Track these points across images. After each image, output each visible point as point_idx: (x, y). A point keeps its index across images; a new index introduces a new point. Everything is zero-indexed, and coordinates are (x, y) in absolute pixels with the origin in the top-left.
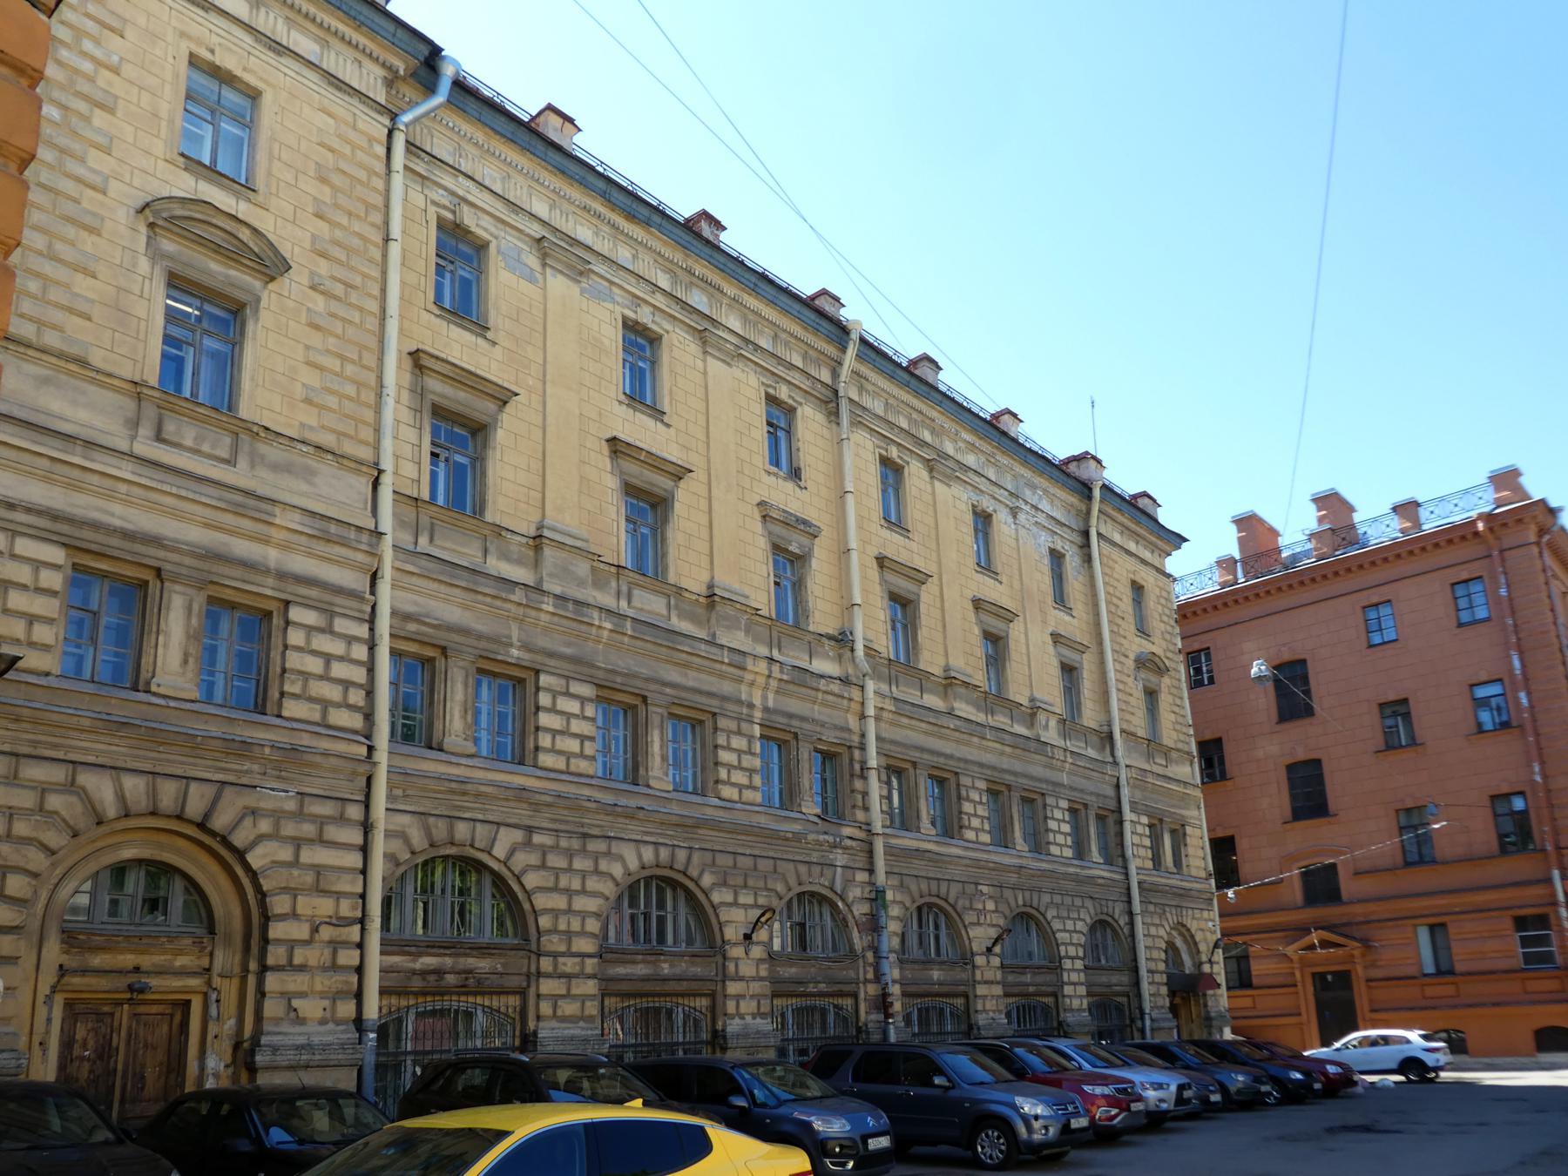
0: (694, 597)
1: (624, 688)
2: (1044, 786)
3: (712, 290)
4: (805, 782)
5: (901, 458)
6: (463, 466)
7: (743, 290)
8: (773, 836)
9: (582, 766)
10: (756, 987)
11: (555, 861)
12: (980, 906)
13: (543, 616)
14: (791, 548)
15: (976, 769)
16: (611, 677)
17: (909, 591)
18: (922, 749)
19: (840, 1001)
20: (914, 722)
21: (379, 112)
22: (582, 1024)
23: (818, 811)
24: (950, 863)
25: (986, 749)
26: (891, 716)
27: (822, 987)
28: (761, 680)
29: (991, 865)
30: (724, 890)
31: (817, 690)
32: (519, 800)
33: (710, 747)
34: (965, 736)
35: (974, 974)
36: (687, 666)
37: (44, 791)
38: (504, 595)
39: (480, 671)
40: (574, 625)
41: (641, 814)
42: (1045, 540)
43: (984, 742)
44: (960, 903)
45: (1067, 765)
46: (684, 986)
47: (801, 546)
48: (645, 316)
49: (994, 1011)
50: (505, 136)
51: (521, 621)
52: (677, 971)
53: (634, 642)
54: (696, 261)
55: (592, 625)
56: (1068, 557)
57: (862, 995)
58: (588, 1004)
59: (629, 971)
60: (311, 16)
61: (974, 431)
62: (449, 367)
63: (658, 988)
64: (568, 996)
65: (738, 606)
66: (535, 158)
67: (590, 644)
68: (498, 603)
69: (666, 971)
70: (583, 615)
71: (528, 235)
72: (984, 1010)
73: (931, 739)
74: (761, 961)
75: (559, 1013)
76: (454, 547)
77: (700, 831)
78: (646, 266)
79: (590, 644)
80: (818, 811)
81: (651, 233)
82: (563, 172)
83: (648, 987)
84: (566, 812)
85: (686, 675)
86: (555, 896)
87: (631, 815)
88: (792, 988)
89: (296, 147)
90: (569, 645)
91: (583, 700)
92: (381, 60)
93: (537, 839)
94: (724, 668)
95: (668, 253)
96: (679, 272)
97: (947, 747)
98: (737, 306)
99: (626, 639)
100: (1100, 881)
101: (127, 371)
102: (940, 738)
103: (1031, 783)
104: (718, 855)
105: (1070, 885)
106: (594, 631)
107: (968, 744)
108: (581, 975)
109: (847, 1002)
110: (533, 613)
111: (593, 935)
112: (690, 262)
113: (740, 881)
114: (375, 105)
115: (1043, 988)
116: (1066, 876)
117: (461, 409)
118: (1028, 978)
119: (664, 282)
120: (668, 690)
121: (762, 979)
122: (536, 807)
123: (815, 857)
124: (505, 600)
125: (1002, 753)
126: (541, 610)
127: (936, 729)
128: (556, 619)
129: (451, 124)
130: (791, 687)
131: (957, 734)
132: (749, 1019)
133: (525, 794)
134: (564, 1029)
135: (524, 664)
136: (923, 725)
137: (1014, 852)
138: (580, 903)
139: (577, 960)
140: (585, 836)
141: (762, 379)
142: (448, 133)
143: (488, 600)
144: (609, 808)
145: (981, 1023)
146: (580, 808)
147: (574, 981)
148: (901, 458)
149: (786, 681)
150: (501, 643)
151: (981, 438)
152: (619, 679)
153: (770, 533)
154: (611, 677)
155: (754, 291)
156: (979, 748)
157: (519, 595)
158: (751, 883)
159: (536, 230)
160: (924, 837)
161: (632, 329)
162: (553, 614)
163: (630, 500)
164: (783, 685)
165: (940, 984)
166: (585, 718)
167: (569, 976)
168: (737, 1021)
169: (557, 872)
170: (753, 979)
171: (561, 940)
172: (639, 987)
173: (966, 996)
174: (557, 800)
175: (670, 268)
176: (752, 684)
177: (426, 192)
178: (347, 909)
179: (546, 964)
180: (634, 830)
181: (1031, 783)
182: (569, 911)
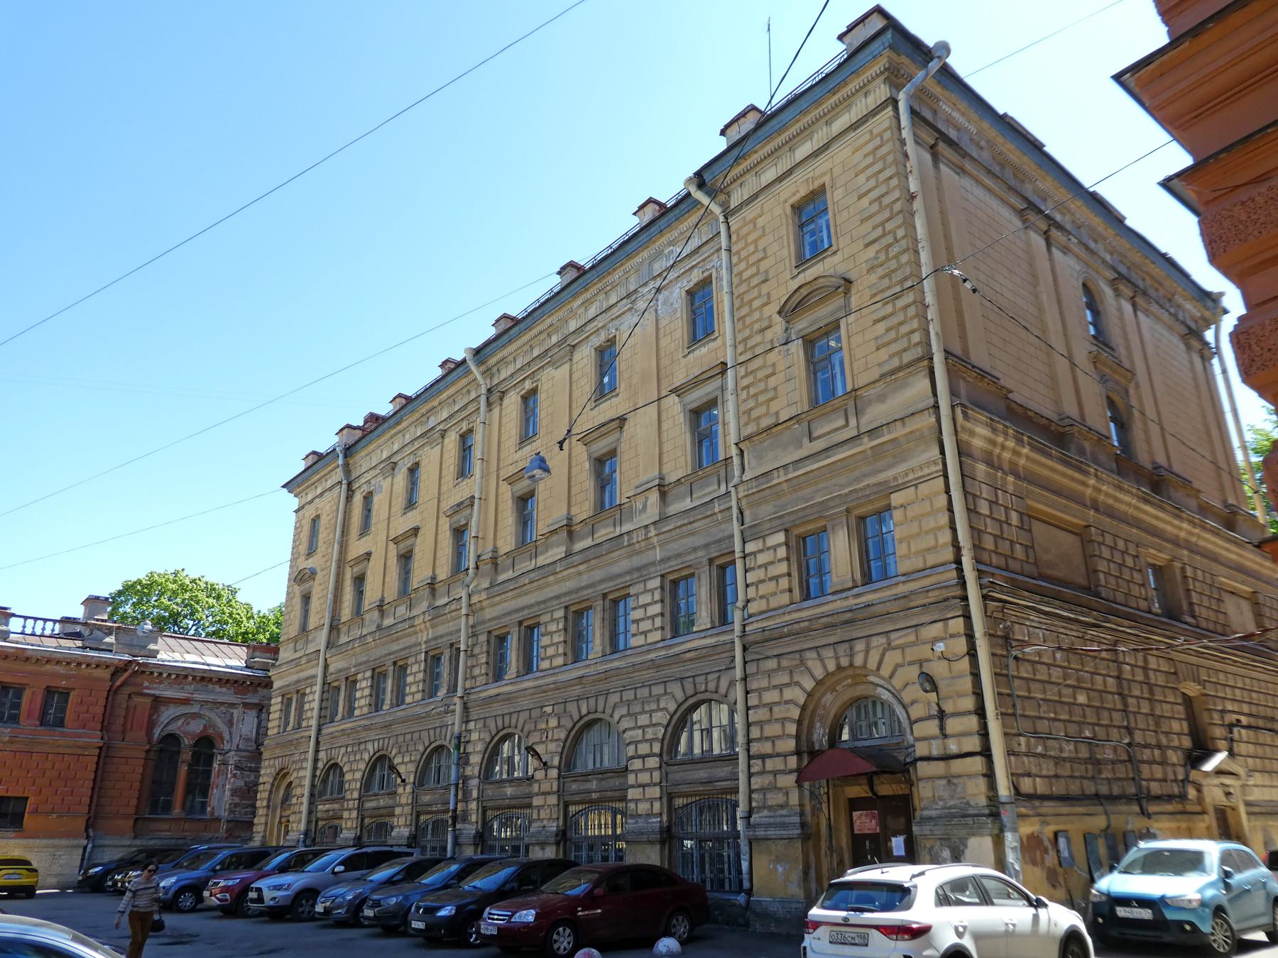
12: (544, 726)
20: (503, 596)
24: (517, 697)
25: (564, 579)
26: (488, 602)
29: (552, 686)
34: (543, 581)
36: (397, 639)
41: (373, 727)
43: (559, 576)
45: (655, 540)
61: (575, 296)
73: (519, 600)
100: (689, 655)
101: (386, 596)
102: (525, 594)
105: (651, 674)
107: (547, 585)
115: (609, 794)
116: (569, 684)
118: (594, 785)
125: (580, 574)
127: (519, 590)
130: (436, 621)
131: (535, 584)
136: (510, 594)
138: (778, 712)
146: (357, 732)
155: (440, 392)
156: (557, 582)
165: (511, 798)
175: (417, 423)
178: (757, 766)
181: (611, 584)
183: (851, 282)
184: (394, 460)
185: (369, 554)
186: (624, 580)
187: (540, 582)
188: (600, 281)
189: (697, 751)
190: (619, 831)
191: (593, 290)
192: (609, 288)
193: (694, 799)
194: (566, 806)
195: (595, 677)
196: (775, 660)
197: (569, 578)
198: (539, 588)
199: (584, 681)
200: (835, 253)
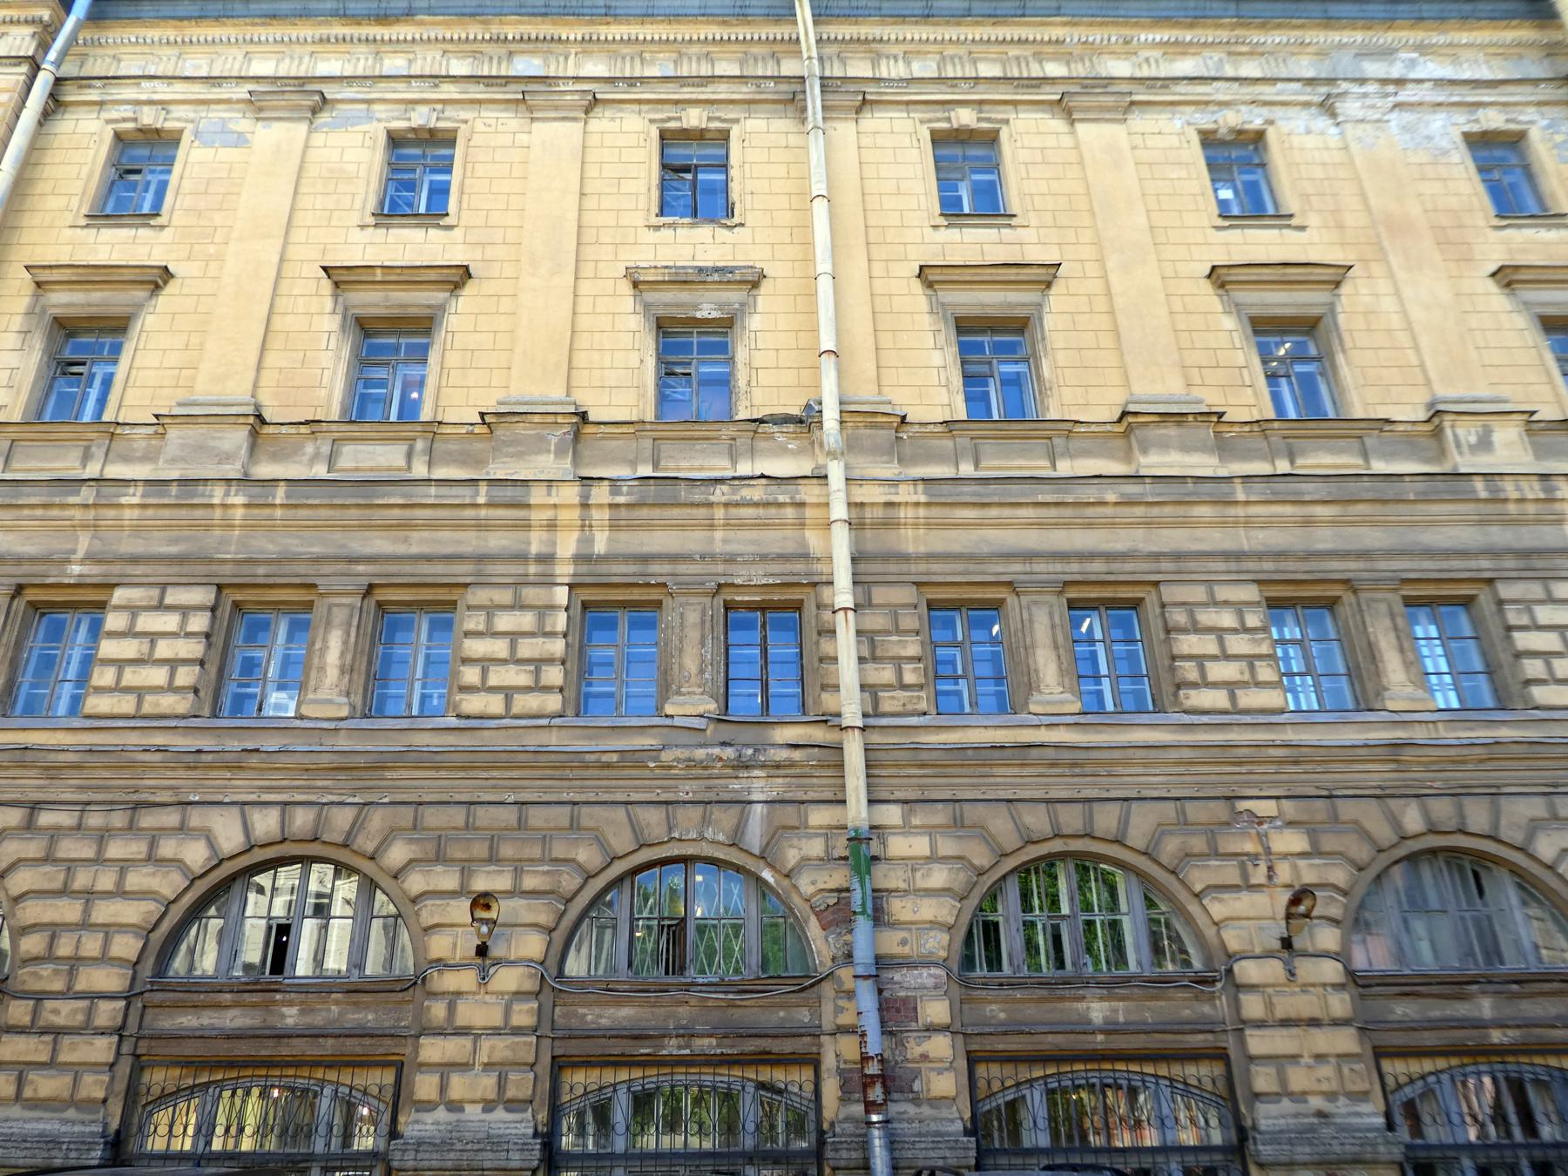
0: (463, 430)
1: (271, 581)
2: (1485, 563)
3: (545, 46)
4: (691, 663)
5: (989, 120)
6: (1310, 375)
7: (592, 23)
8: (572, 764)
9: (168, 703)
10: (492, 1048)
11: (70, 848)
13: (128, 513)
14: (699, 315)
15: (1221, 566)
16: (246, 569)
17: (1009, 305)
18: (1029, 556)
19: (778, 1076)
20: (994, 512)
21: (15, 65)
22: (71, 1113)
23: (711, 707)
24: (1127, 763)
25: (1248, 523)
27: (706, 1045)
28: (572, 515)
30: (439, 868)
31: (710, 505)
32: (22, 765)
33: (219, 640)
35: (1236, 1005)
36: (406, 526)
37: (130, 828)
38: (57, 500)
39: (1409, 602)
40: (183, 513)
41: (254, 760)
42: (1446, 129)
43: (1232, 511)
44: (1170, 848)
45: (240, 512)
46: (329, 1046)
47: (720, 306)
48: (1493, 120)
49: (1331, 1096)
50: (189, 18)
51: (94, 527)
52: (318, 1020)
53: (291, 513)
54: (501, 23)
55: (212, 506)
56: (1535, 134)
57: (829, 1061)
58: (88, 1079)
59: (206, 1021)
60: (15, 19)
62: (69, 271)
63: (266, 1050)
64: (51, 1064)
65: (537, 419)
66: (235, 21)
67: (218, 532)
68: (54, 513)
69: (290, 1021)
70: (194, 496)
71: (239, 101)
72: (1284, 1093)
74: (519, 995)
75: (28, 1092)
76: (40, 465)
77: (388, 774)
78: (428, 61)
79: (218, 532)
80: (711, 707)
81: (422, 23)
82: (274, 16)
83: (243, 1049)
84: (107, 774)
85: (406, 540)
86: (63, 903)
87: (235, 764)
88: (616, 1048)
89: (471, 143)
90: (176, 541)
91: (1239, 607)
92: (22, 19)
93: (46, 818)
94: (483, 513)
95: (457, 32)
96: (485, 48)
97: (1120, 541)
98: (595, 47)
99: (279, 513)
103: (1428, 564)
104: (1189, 806)
106: (218, 513)
108: (87, 1029)
109: (797, 1078)
110: (112, 513)
111: (120, 962)
112: (495, 29)
113: (480, 850)
114: (8, 61)
117: (93, 311)
119: (460, 67)
120: (361, 568)
121: (518, 1031)
122: (52, 771)
123: (686, 790)
124: (63, 506)
125: (1308, 522)
126: (121, 506)
128: (150, 512)
129: (133, 39)
130: (644, 512)
132: (473, 1112)
133: (29, 756)
134: (30, 1120)
135: (89, 581)
137: (1383, 716)
138: (104, 912)
139: (84, 1004)
140: (138, 806)
141: (917, 115)
142: (138, 49)
143: (39, 512)
144: (190, 758)
145: (1264, 1124)
146: (132, 765)
147: (66, 1041)
148: (989, 120)
149: (628, 505)
150: (53, 561)
151: (1191, 26)
152: (261, 570)
153: (1525, 303)
154: (246, 569)
156: (1222, 523)
157: (87, 494)
158: (507, 851)
159: (241, 92)
160: (1035, 720)
161: (1481, 143)
162: (143, 506)
163: (1553, 337)
164: (623, 513)
165: (1110, 1029)
166: (1247, 630)
167: (57, 1032)
168: (441, 1114)
169: (71, 865)
170: (496, 1032)
171: (56, 972)
172: (223, 1049)
173: (1221, 1056)
174: (89, 757)
175: (467, 47)
176: (552, 526)
177: (912, 115)
179: (107, 1013)
180: (242, 787)
181: (1428, 564)
182: (85, 925)
183: (470, 276)
184: (331, 91)
185: (164, 275)
186: (1473, 564)
187: (1155, 511)
188: (1233, 27)
189: (373, 967)
190: (217, 1145)
191: (1209, 35)
192: (1244, 49)
193: (1038, 1073)
194: (139, 1065)
195: (1452, 752)
196: (462, 810)
197: (1267, 523)
198: (1148, 524)
199: (1407, 754)
200: (162, 227)
